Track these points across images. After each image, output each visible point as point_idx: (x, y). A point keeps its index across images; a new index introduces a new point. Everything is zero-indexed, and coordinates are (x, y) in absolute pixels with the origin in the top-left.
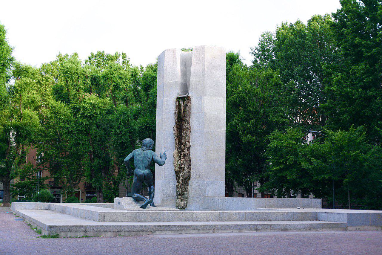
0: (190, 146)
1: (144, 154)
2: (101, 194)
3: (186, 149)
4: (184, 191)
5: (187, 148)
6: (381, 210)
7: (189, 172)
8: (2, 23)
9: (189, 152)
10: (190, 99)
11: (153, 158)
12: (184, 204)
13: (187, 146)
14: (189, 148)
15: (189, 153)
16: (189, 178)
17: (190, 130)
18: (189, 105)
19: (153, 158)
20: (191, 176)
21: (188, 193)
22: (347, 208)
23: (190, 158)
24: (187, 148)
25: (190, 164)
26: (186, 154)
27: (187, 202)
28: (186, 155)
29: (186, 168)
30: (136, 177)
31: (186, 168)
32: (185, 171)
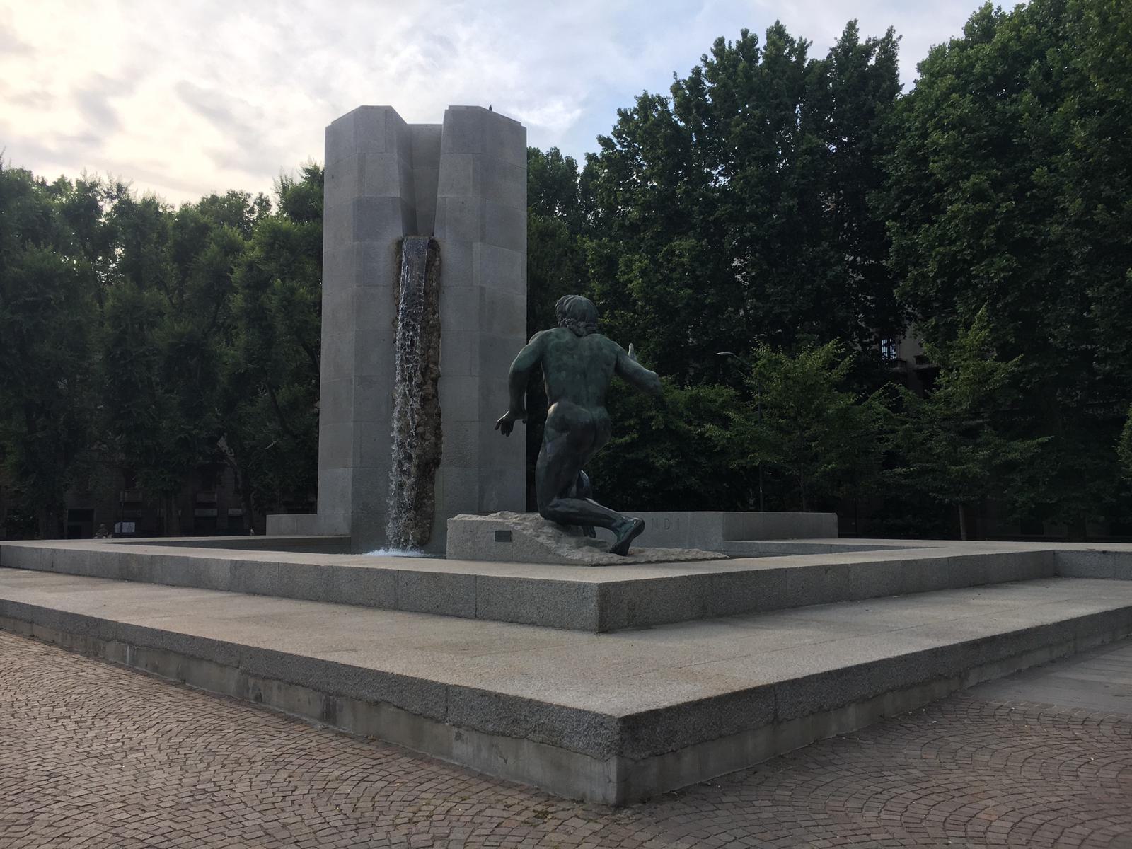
0: (440, 376)
1: (591, 349)
2: (51, 514)
3: (430, 381)
4: (424, 498)
5: (432, 379)
6: (1129, 542)
7: (436, 445)
8: (13, 162)
9: (436, 391)
10: (439, 247)
11: (617, 359)
12: (423, 533)
13: (433, 376)
14: (435, 381)
15: (435, 396)
16: (436, 463)
17: (439, 330)
18: (437, 263)
19: (617, 359)
20: (443, 457)
21: (433, 504)
22: (955, 536)
23: (440, 409)
24: (432, 379)
25: (440, 424)
26: (430, 398)
27: (430, 528)
28: (429, 400)
29: (428, 434)
30: (565, 435)
31: (428, 435)
32: (427, 443)
